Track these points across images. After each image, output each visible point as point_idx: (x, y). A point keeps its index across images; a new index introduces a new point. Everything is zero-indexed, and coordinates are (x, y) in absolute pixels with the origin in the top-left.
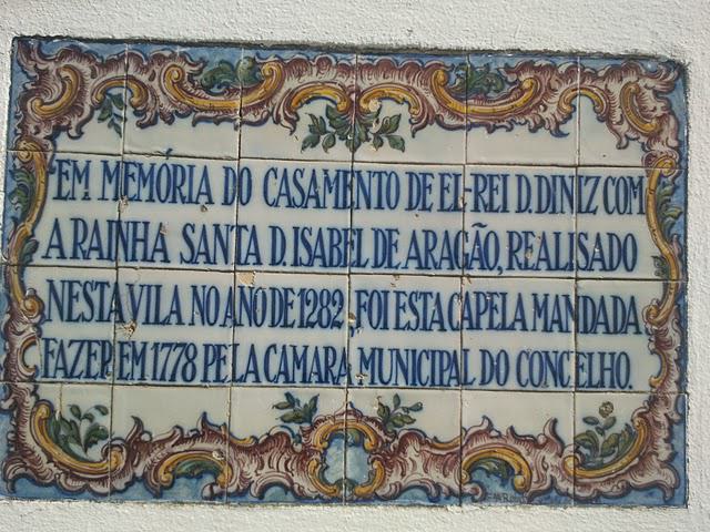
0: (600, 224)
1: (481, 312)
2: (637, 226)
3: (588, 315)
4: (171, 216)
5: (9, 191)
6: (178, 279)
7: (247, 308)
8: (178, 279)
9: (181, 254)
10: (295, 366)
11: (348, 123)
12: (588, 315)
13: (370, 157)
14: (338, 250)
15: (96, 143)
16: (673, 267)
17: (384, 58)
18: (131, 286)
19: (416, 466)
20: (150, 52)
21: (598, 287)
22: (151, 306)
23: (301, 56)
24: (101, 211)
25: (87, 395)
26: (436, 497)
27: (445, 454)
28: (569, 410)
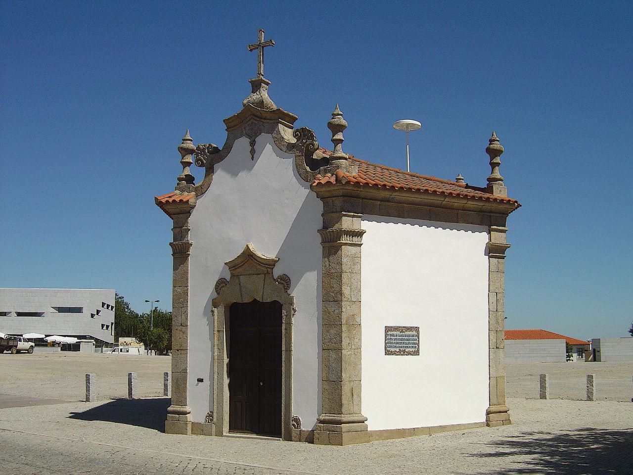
0: (415, 338)
1: (409, 343)
2: (417, 338)
3: (414, 343)
4: (393, 337)
5: (189, 214)
6: (394, 341)
7: (397, 343)
8: (394, 341)
9: (76, 416)
10: (399, 347)
11: (402, 331)
12: (414, 343)
13: (403, 333)
14: (402, 340)
15: (389, 333)
16: (419, 341)
17: (404, 327)
18: (360, 234)
19: (406, 353)
20: (392, 327)
21: (415, 342)
22: (392, 343)
23: (399, 327)
24: (390, 337)
25: (389, 349)
26: (407, 355)
27: (407, 352)
28: (413, 349)
